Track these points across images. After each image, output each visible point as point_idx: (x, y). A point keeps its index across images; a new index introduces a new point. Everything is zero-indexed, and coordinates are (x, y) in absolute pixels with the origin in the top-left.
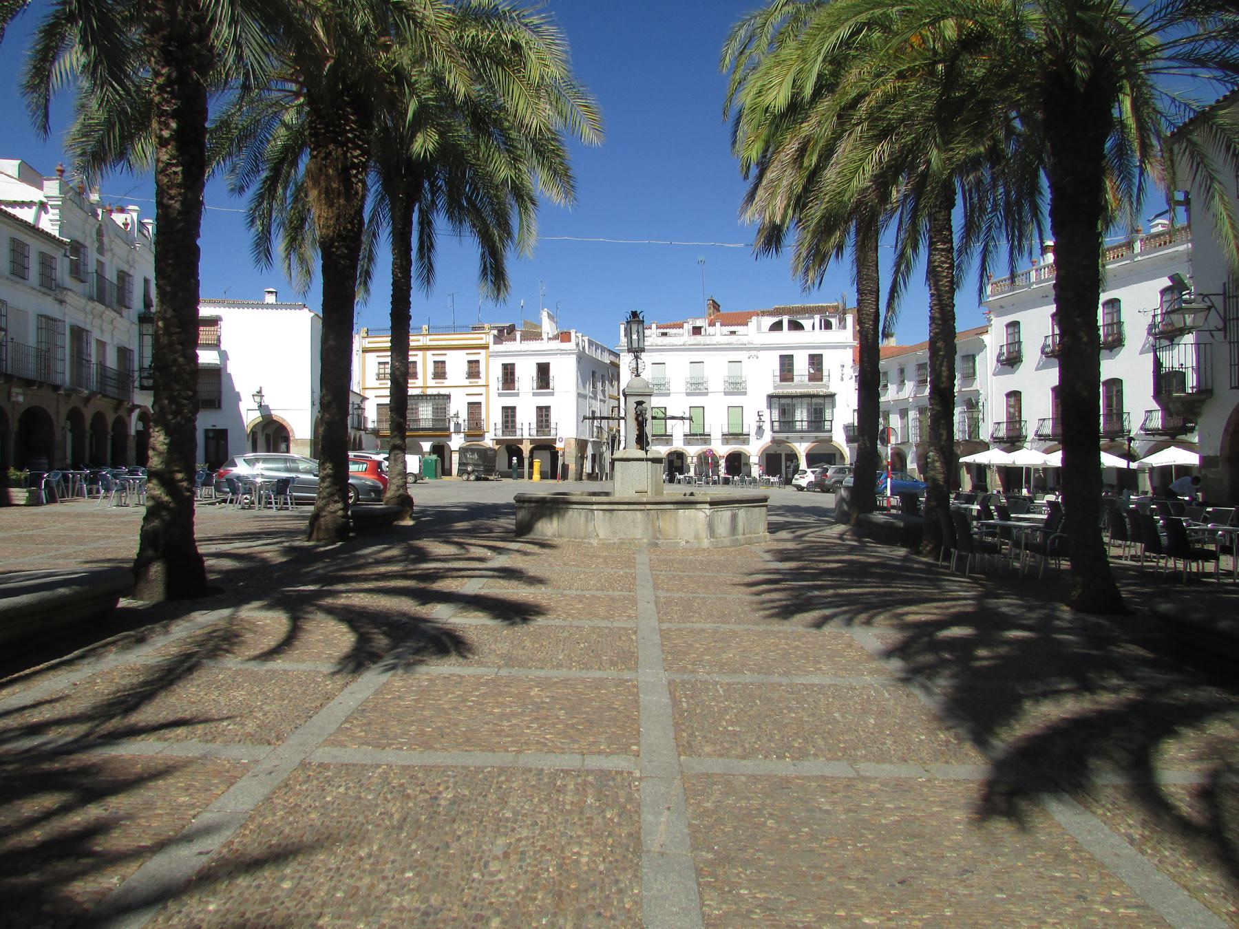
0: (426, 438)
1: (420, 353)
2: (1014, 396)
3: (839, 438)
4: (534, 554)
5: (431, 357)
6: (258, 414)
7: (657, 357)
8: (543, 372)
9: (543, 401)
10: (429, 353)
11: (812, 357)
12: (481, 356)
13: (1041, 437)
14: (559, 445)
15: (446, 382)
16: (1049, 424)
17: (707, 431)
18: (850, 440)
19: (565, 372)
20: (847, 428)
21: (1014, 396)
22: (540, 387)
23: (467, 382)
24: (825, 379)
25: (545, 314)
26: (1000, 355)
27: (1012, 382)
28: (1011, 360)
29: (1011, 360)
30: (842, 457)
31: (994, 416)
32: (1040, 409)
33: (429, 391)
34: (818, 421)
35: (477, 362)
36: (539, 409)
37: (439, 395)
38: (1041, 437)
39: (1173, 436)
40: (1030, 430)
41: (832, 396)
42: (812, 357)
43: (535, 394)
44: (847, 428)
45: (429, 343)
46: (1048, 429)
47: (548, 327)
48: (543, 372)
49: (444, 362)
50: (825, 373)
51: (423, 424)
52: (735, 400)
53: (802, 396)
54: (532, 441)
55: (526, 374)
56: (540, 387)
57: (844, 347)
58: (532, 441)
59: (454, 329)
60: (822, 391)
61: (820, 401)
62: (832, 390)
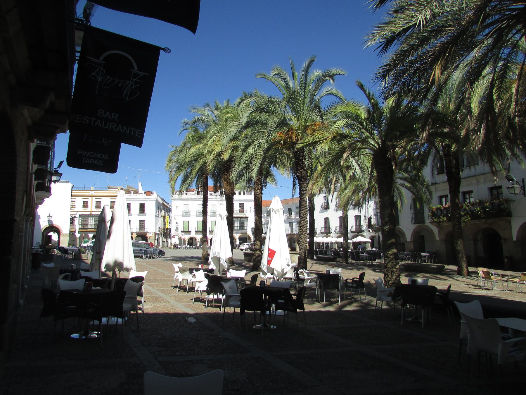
0: (91, 232)
1: (90, 198)
2: (327, 220)
3: (250, 233)
4: (445, 280)
5: (94, 199)
6: (47, 224)
7: (214, 203)
8: (142, 206)
9: (142, 218)
10: (94, 198)
11: (240, 204)
12: (89, 199)
13: (322, 233)
14: (148, 235)
15: (75, 210)
16: (338, 228)
17: (190, 230)
18: (253, 233)
19: (151, 207)
20: (252, 229)
21: (327, 220)
22: (140, 213)
23: (82, 210)
24: (245, 212)
25: (140, 184)
26: (322, 206)
27: (326, 215)
28: (326, 207)
29: (326, 207)
30: (250, 238)
31: (319, 225)
32: (335, 224)
33: (93, 213)
34: (242, 227)
35: (87, 202)
36: (140, 221)
37: (83, 215)
38: (322, 233)
39: (358, 233)
40: (333, 230)
41: (247, 218)
42: (240, 204)
43: (138, 215)
44: (252, 229)
45: (94, 194)
46: (338, 230)
47: (141, 190)
48: (142, 206)
49: (100, 202)
50: (245, 210)
51: (90, 227)
52: (186, 219)
53: (237, 218)
54: (137, 233)
55: (135, 208)
56: (140, 213)
57: (251, 201)
58: (137, 233)
59: (84, 188)
60: (244, 216)
61: (243, 219)
62: (247, 216)
